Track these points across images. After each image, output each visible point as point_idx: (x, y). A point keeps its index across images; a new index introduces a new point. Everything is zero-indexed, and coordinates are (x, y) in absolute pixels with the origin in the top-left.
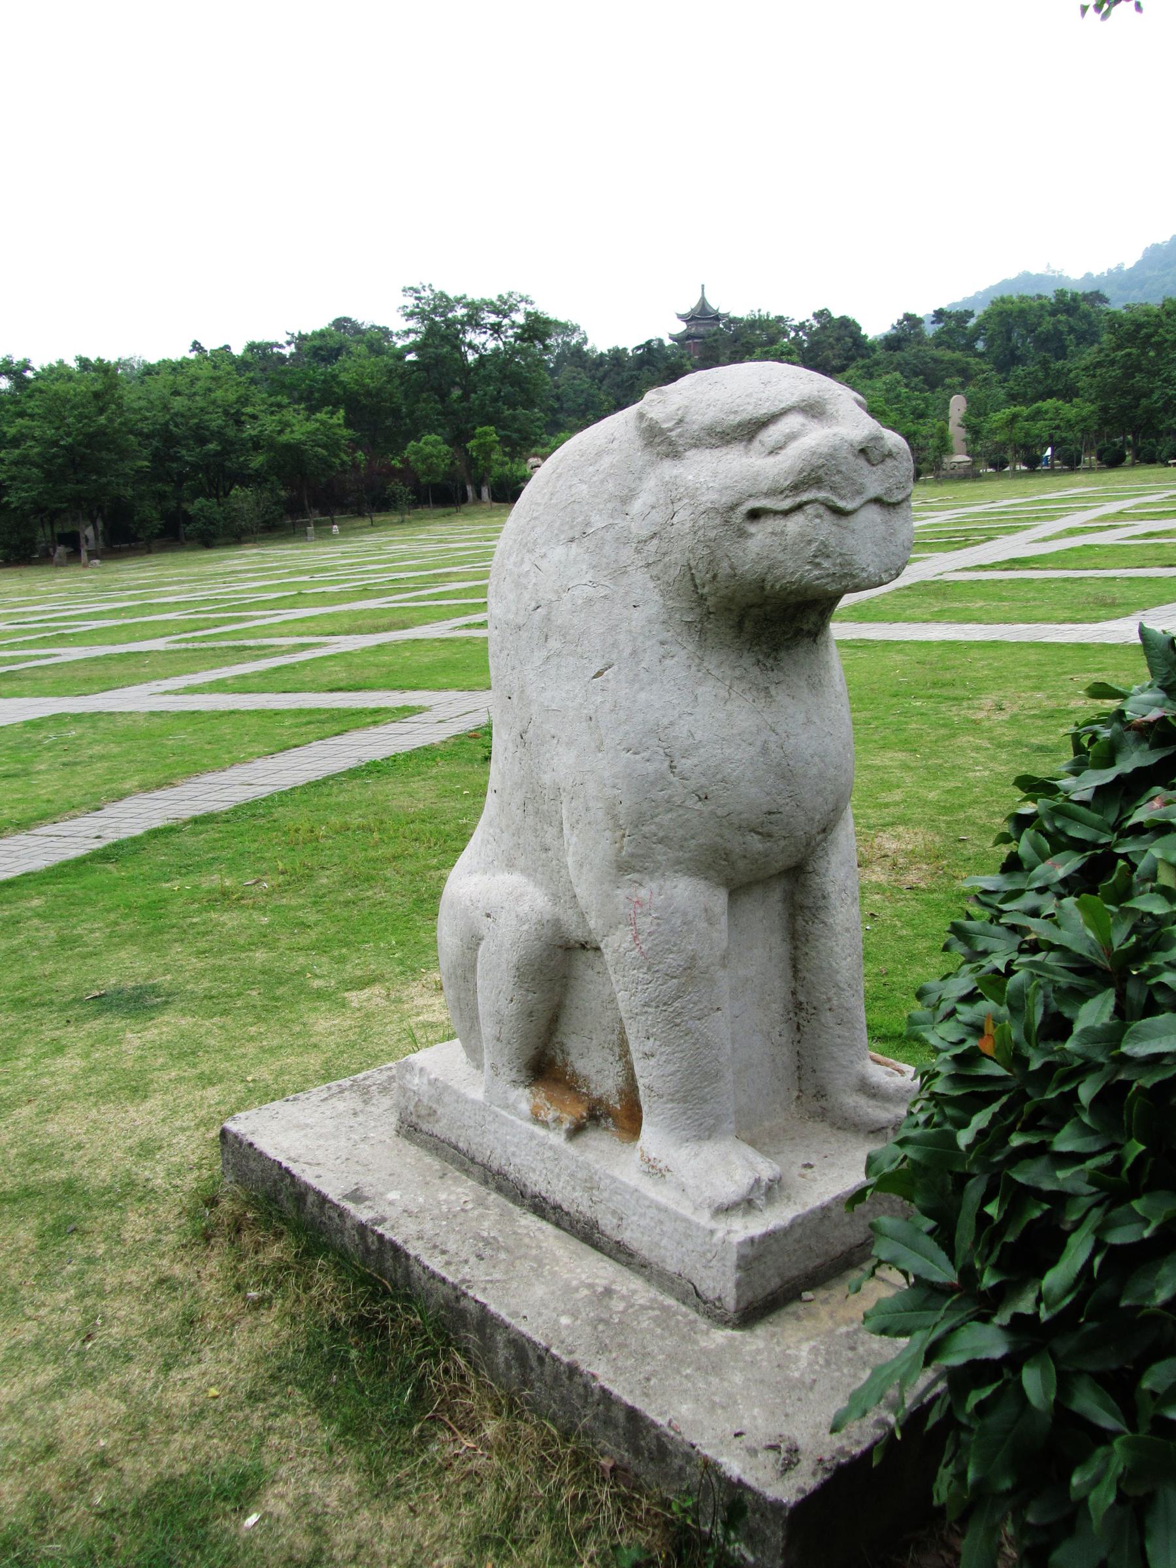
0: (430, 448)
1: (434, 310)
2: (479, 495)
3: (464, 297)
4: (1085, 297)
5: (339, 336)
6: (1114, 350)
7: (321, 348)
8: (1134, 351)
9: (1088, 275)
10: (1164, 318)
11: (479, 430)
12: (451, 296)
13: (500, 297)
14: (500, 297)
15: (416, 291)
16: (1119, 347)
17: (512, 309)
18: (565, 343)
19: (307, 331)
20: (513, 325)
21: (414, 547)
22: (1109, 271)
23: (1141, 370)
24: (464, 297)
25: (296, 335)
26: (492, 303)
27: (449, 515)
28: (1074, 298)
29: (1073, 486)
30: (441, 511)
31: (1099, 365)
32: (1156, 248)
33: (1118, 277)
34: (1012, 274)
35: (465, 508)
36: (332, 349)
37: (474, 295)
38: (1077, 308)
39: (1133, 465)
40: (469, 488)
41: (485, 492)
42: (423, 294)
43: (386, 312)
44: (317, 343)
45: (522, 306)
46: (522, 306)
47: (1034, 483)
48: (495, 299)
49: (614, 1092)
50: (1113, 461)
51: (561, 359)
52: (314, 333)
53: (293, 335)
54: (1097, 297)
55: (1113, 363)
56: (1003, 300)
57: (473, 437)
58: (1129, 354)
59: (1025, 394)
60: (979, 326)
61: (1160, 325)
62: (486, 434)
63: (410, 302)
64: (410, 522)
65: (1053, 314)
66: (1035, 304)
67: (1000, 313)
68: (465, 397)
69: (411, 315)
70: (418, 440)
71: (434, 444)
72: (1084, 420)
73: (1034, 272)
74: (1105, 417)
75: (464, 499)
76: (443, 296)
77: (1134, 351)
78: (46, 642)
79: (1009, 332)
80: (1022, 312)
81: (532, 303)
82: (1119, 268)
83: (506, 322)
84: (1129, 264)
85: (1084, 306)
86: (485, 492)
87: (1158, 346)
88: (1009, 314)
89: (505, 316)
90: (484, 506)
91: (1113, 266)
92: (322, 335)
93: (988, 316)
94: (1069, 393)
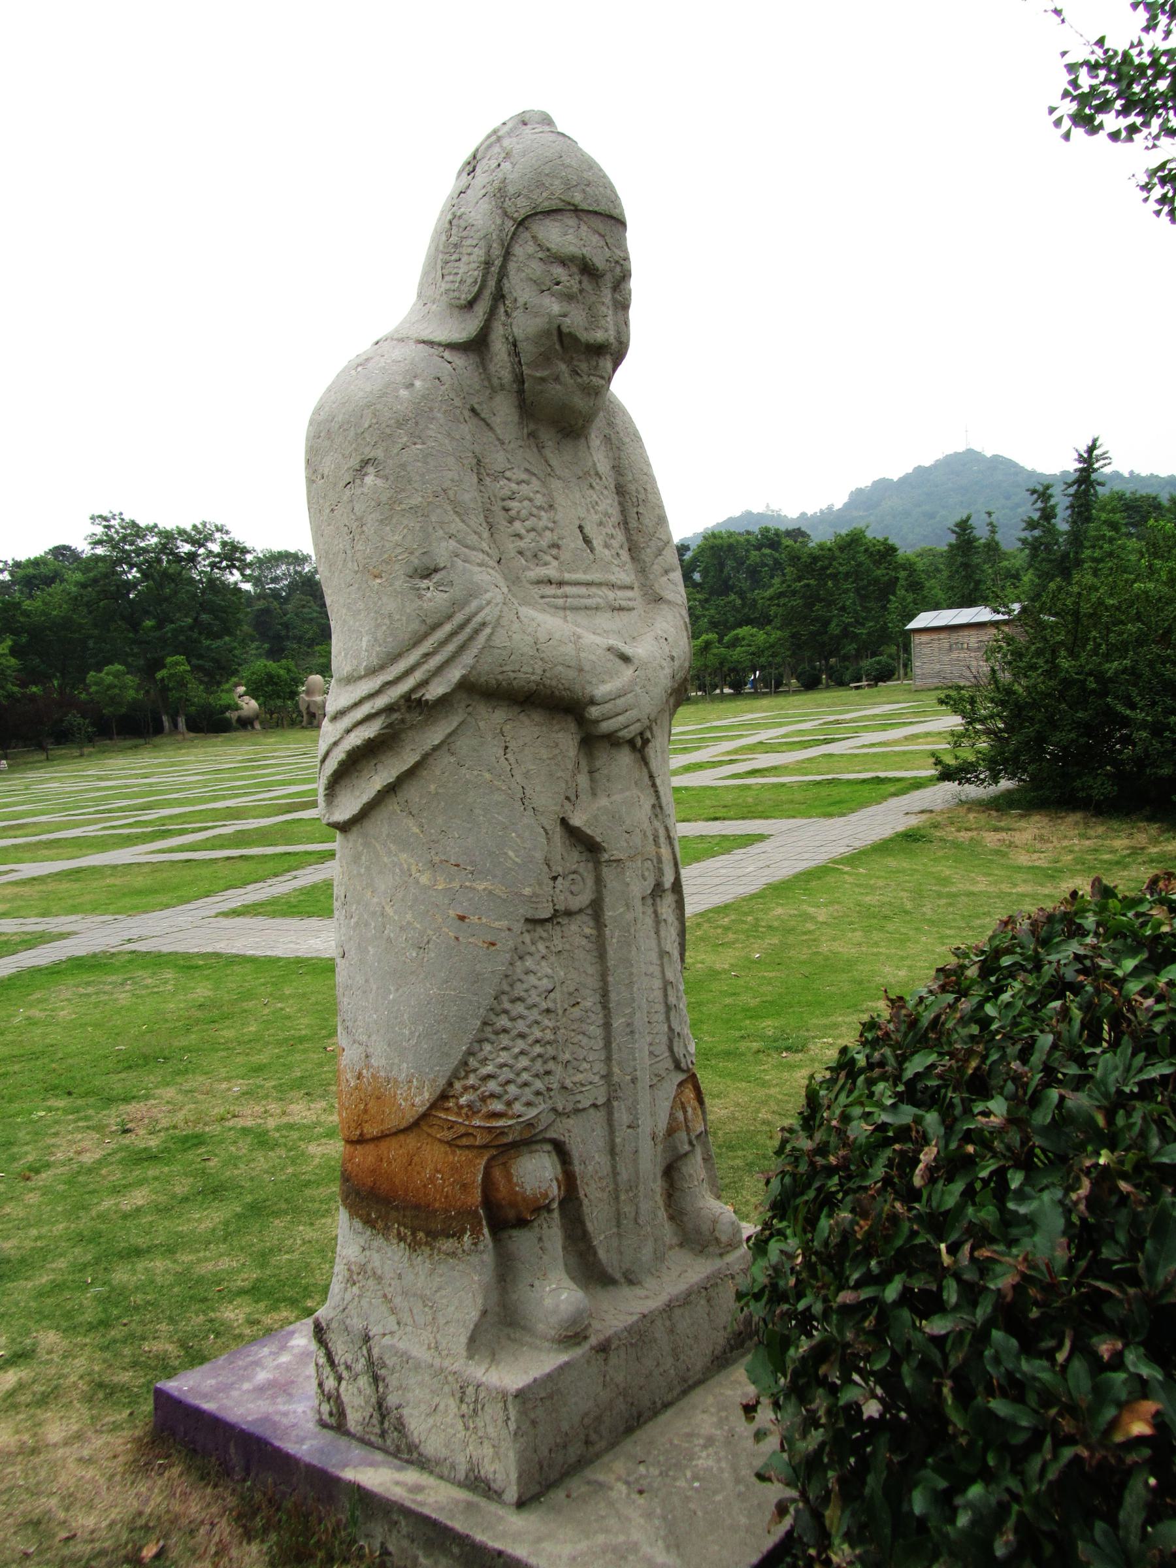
0: (114, 680)
1: (124, 539)
2: (176, 726)
3: (156, 526)
4: (788, 534)
5: (54, 564)
6: (795, 581)
7: (34, 577)
8: (812, 582)
9: (803, 514)
10: (837, 553)
11: (169, 660)
12: (143, 525)
13: (195, 527)
14: (195, 527)
15: (105, 519)
16: (800, 579)
17: (209, 538)
18: (296, 572)
19: (22, 557)
20: (210, 553)
21: (69, 786)
22: (821, 511)
23: (820, 600)
24: (156, 526)
25: (10, 562)
26: (185, 532)
27: (136, 747)
28: (777, 534)
29: (751, 711)
30: (129, 743)
31: (781, 595)
32: (859, 492)
33: (827, 516)
34: (736, 513)
35: (157, 740)
36: (46, 577)
37: (168, 523)
38: (779, 543)
39: (828, 687)
40: (165, 718)
41: (181, 722)
42: (112, 522)
43: (80, 538)
44: (31, 571)
45: (218, 535)
46: (218, 535)
47: (741, 704)
48: (189, 528)
49: (755, 1101)
50: (810, 684)
51: (292, 587)
52: (29, 560)
53: (6, 563)
54: (797, 534)
55: (794, 593)
56: (714, 536)
57: (164, 666)
58: (808, 585)
59: (727, 621)
60: (695, 559)
61: (833, 558)
62: (177, 663)
63: (99, 530)
64: (90, 755)
65: (758, 548)
66: (742, 539)
67: (712, 548)
68: (160, 626)
69: (100, 542)
70: (100, 671)
71: (117, 675)
72: (772, 646)
73: (755, 511)
74: (797, 644)
75: (158, 730)
76: (134, 524)
77: (812, 582)
78: (410, 774)
79: (722, 565)
80: (731, 547)
81: (227, 533)
82: (830, 508)
83: (202, 551)
84: (838, 506)
85: (788, 542)
86: (181, 722)
87: (834, 576)
88: (720, 548)
89: (201, 545)
90: (180, 737)
91: (824, 507)
92: (36, 563)
93: (702, 550)
94: (762, 621)
